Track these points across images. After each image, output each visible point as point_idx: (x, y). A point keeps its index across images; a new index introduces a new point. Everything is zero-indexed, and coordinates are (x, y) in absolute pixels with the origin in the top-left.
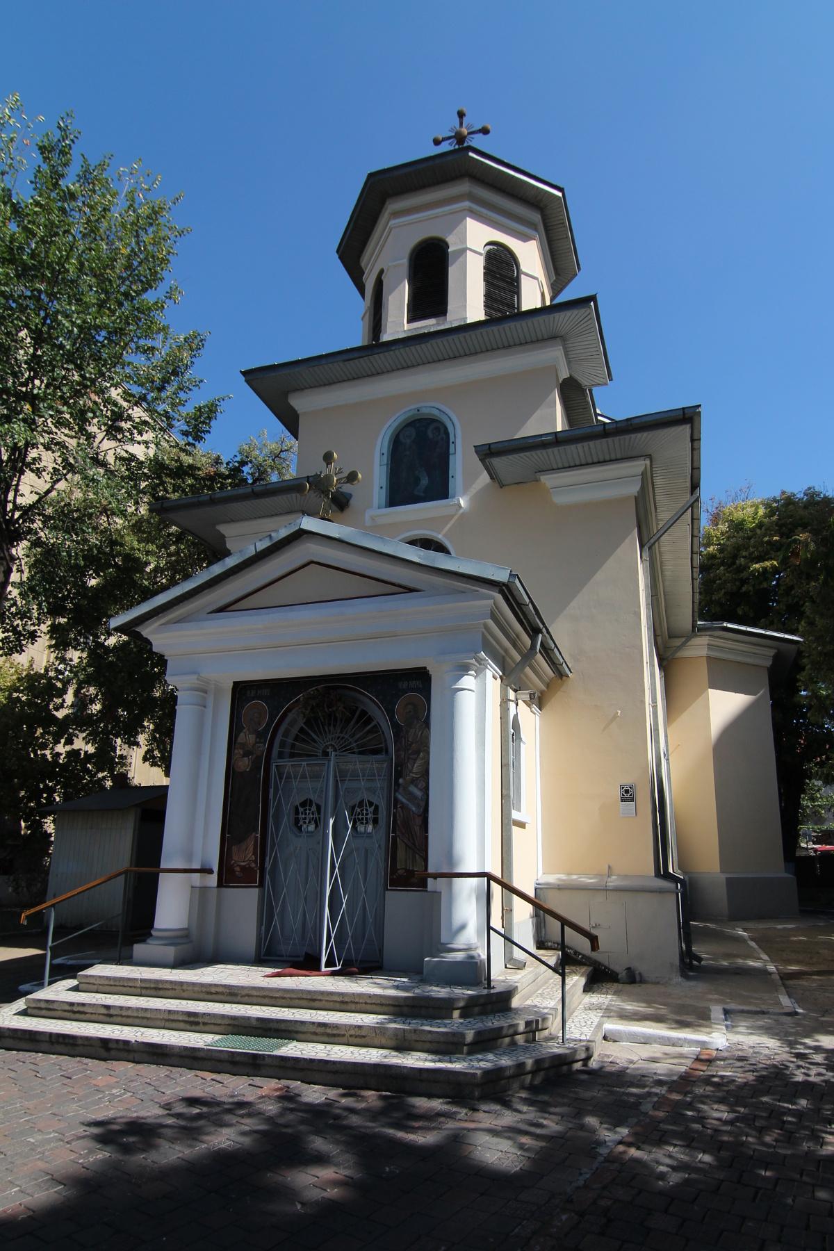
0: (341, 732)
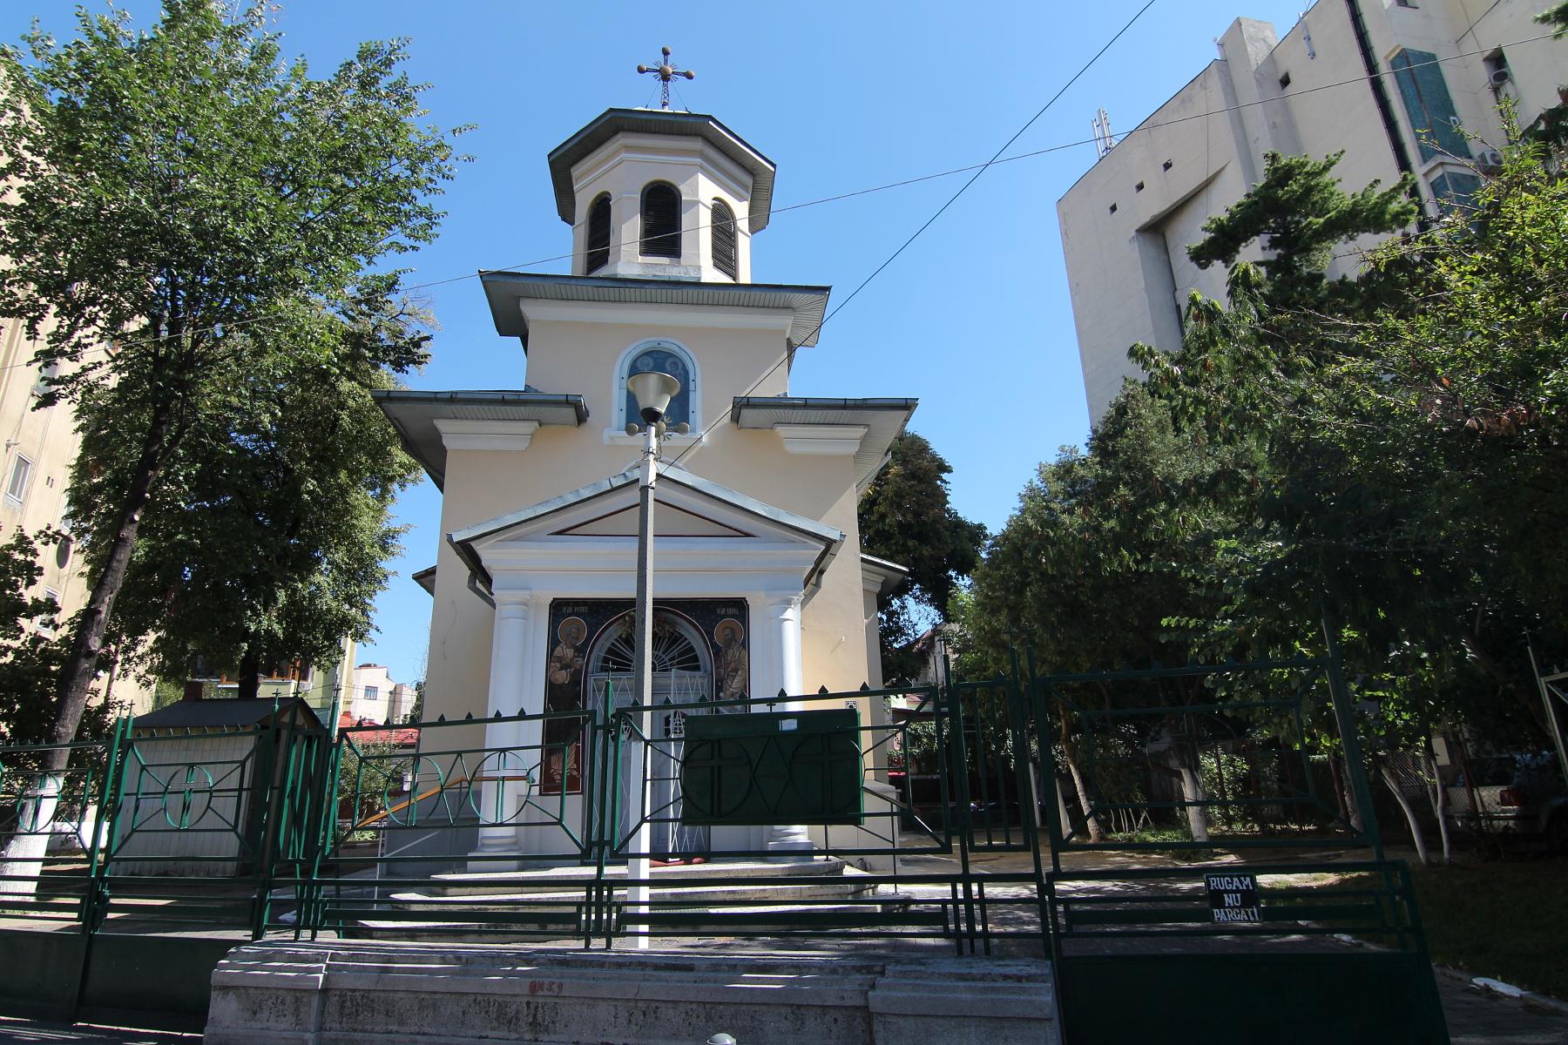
0: (664, 653)
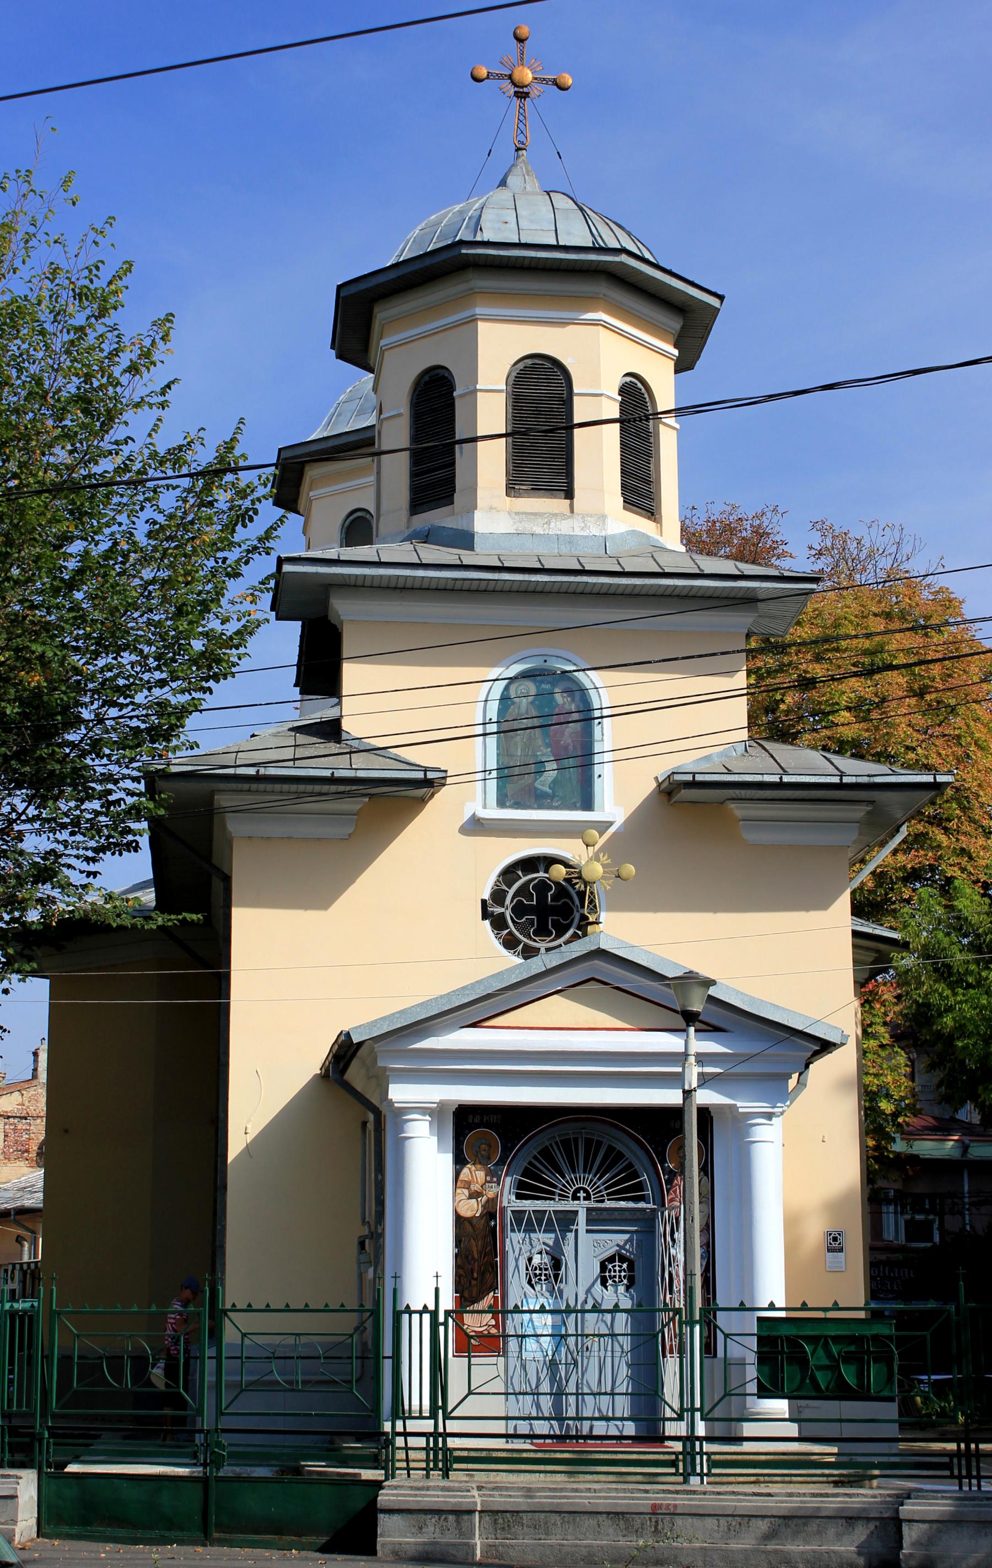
0: (608, 1194)
